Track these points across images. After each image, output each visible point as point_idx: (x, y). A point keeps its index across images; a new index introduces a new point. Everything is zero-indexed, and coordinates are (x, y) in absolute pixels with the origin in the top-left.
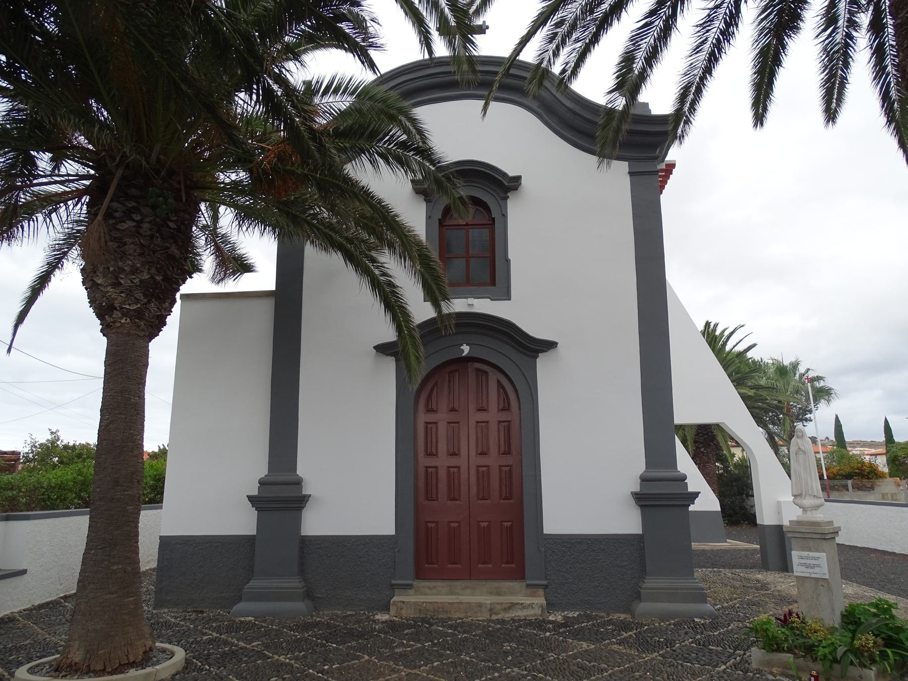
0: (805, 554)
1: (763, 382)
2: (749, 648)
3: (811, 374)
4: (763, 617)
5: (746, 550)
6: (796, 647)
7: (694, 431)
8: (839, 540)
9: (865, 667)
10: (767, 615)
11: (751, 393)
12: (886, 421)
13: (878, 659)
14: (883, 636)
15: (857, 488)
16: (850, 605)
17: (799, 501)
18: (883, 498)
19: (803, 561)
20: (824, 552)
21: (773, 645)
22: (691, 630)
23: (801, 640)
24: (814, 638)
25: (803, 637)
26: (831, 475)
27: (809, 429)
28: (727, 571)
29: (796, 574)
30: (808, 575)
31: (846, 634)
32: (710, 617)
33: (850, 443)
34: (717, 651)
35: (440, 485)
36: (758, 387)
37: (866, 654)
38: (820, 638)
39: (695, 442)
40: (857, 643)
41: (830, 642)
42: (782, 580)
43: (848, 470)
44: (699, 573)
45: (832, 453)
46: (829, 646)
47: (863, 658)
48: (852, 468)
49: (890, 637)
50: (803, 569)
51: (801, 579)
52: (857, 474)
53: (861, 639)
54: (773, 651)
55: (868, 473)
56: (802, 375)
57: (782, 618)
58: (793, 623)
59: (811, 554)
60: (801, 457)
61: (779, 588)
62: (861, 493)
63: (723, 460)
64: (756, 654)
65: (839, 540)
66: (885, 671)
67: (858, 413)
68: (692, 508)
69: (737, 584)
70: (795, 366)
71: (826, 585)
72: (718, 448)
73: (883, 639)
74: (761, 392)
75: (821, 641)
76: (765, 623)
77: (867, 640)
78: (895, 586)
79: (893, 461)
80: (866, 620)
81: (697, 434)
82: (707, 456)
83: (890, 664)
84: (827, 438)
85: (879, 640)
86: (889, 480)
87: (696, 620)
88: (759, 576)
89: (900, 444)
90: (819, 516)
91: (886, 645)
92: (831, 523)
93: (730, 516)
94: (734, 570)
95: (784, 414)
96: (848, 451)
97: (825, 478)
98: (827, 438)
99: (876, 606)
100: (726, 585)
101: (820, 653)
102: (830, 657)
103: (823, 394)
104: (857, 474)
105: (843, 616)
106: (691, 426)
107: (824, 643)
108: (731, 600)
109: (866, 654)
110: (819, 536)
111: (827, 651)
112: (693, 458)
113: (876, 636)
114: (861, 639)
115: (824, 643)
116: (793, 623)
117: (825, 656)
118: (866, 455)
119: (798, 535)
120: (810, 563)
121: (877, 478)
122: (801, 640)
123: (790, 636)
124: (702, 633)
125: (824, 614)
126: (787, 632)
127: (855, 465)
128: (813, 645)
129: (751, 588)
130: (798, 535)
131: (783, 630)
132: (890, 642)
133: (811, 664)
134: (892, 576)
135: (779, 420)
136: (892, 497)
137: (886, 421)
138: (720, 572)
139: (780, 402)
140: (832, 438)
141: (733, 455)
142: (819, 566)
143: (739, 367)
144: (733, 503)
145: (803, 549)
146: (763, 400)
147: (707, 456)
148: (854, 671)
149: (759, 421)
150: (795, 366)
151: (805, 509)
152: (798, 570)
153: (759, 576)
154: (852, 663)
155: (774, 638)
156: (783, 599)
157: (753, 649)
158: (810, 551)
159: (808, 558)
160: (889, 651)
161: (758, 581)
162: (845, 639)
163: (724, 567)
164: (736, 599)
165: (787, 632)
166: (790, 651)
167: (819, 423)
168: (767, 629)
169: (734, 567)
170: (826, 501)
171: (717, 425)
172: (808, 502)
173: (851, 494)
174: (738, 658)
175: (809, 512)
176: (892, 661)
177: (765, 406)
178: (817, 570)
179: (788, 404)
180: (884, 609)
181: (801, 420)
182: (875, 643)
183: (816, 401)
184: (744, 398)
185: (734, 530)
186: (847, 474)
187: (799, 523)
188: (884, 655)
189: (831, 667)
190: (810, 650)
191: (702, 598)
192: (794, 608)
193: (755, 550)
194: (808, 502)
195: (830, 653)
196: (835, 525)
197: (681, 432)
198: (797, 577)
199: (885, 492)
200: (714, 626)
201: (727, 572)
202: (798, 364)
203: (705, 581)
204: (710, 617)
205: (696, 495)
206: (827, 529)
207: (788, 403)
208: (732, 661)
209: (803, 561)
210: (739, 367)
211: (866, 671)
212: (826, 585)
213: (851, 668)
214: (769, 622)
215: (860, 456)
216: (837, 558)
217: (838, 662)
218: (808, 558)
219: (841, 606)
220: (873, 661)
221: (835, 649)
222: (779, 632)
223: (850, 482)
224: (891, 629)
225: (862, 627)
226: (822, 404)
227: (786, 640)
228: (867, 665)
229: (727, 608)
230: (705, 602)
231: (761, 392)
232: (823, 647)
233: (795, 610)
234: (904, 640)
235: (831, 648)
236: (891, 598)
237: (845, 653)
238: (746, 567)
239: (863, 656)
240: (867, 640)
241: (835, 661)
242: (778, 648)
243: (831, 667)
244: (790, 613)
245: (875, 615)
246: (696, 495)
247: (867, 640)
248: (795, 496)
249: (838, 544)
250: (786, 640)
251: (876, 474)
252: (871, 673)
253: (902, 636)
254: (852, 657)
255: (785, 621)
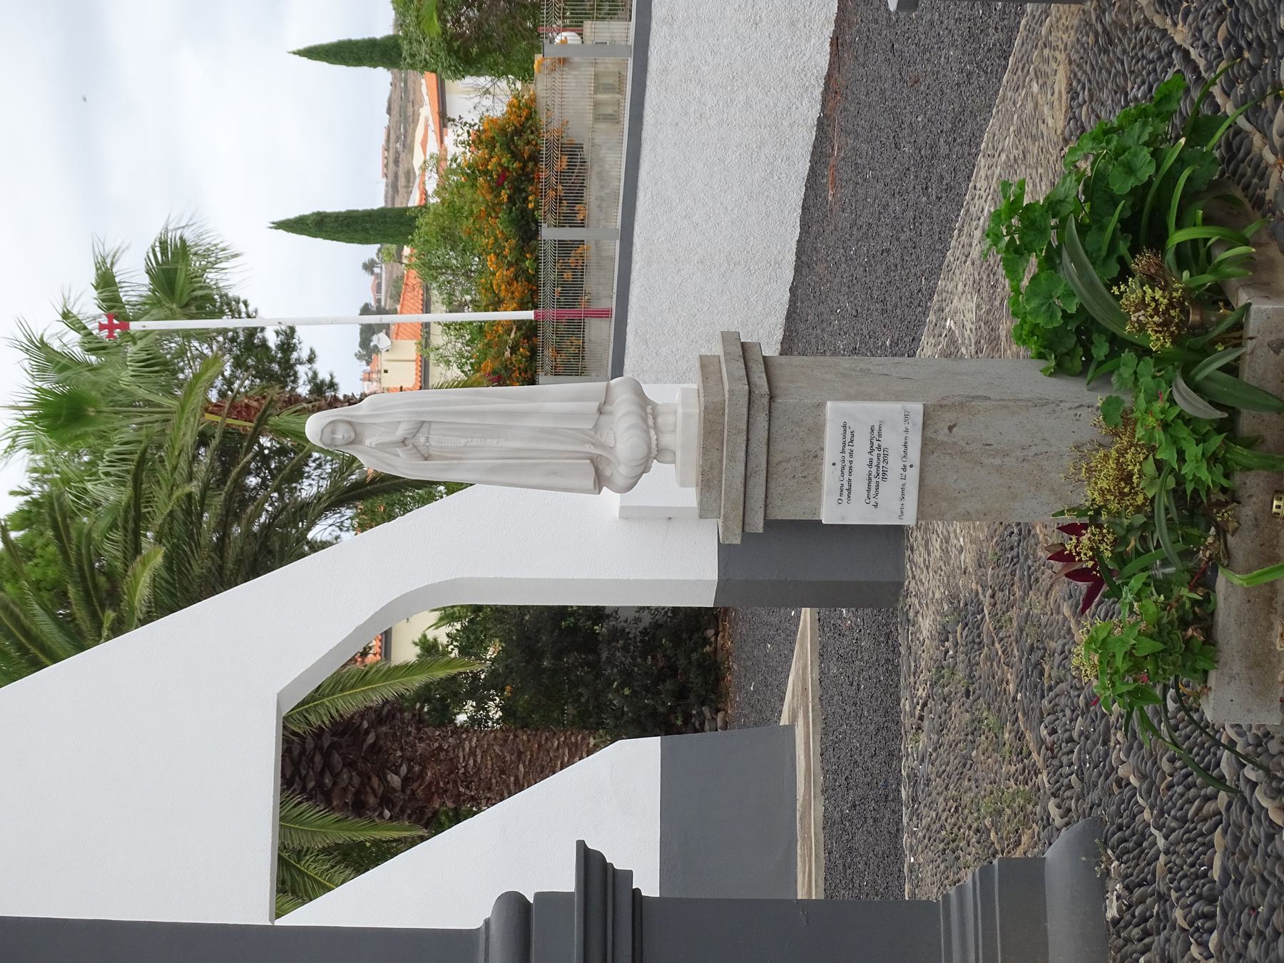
0: (830, 477)
1: (109, 493)
2: (1202, 726)
3: (89, 307)
4: (1083, 659)
5: (823, 654)
6: (1186, 555)
7: (311, 812)
8: (771, 349)
9: (1239, 326)
10: (1086, 643)
11: (154, 556)
12: (313, 53)
13: (1208, 279)
14: (1123, 248)
15: (571, 206)
16: (1021, 340)
17: (621, 472)
18: (614, 119)
19: (859, 487)
20: (820, 406)
21: (1187, 640)
22: (1157, 941)
23: (1161, 533)
24: (1149, 489)
25: (1148, 525)
26: (518, 287)
27: (331, 354)
28: (908, 746)
29: (909, 519)
30: (913, 474)
31: (1126, 372)
32: (1096, 856)
33: (393, 188)
34: (1228, 853)
35: (743, 454)
36: (133, 520)
37: (1194, 317)
38: (1150, 468)
39: (359, 808)
40: (1157, 341)
41: (1159, 435)
42: (936, 544)
43: (499, 225)
44: (923, 876)
45: (431, 271)
46: (1175, 441)
47: (1203, 331)
48: (492, 209)
49: (1127, 225)
50: (889, 490)
51: (930, 499)
52: (518, 194)
53: (1142, 327)
54: (1210, 639)
55: (515, 156)
56: (93, 346)
57: (1083, 586)
58: (1097, 552)
59: (831, 452)
60: (436, 440)
61: (968, 559)
62: (593, 192)
63: (442, 699)
64: (1226, 704)
65: (771, 349)
66: (1248, 262)
67: (263, 142)
68: (648, 883)
69: (960, 718)
70: (46, 357)
71: (949, 417)
72: (386, 715)
73: (1135, 250)
74: (163, 504)
75: (1159, 465)
76: (1108, 660)
77: (1141, 304)
78: (944, 149)
79: (465, 56)
80: (1070, 294)
81: (324, 796)
82: (424, 761)
83: (1226, 244)
84: (369, 267)
85: (1141, 263)
86: (541, 86)
87: (1112, 913)
88: (926, 625)
89: (400, 24)
90: (678, 398)
91: (1158, 240)
92: (706, 364)
93: (681, 694)
94: (907, 722)
95: (257, 433)
96: (424, 208)
97: (529, 315)
98: (369, 267)
99: (1016, 253)
100: (966, 762)
101: (1205, 475)
102: (1216, 441)
103: (180, 277)
104: (518, 194)
105: (1060, 370)
106: (286, 821)
107: (1167, 454)
108: (1023, 754)
109: (1194, 317)
110: (759, 481)
111: (1193, 450)
112: (440, 828)
113: (1125, 274)
114: (1142, 327)
115: (1167, 454)
116: (1097, 552)
117: (1212, 459)
118: (440, 150)
119: (758, 493)
120: (864, 456)
121: (535, 130)
122: (1161, 533)
123: (1153, 561)
124: (1162, 898)
125: (1058, 442)
126: (1136, 583)
127: (480, 197)
128: (1178, 493)
129: (972, 665)
130: (758, 493)
131: (1128, 596)
132: (1144, 224)
133: (1247, 512)
134: (907, 149)
135: (282, 451)
136: (608, 89)
137: (313, 53)
138: (913, 777)
139: (203, 439)
140: (370, 251)
141: (429, 648)
142: (876, 433)
143: (37, 586)
144: (627, 677)
145: (813, 481)
146: (191, 509)
147: (424, 761)
148: (1259, 365)
149: (275, 547)
150: (46, 357)
151: (652, 454)
152: (895, 506)
153: (926, 625)
154: (1232, 370)
155: (1159, 631)
156: (1011, 546)
157: (1209, 716)
158: (817, 456)
159: (846, 468)
160: (1177, 237)
161: (944, 634)
162: (1146, 380)
163: (894, 756)
164: (1020, 736)
165: (1136, 583)
166: (1203, 580)
167: (308, 298)
168: (1129, 654)
169: (891, 713)
170: (618, 370)
171: (286, 723)
172: (623, 438)
173: (598, 233)
174: (1250, 773)
175: (667, 440)
176: (1212, 234)
177: (218, 500)
178: (892, 440)
179: (216, 409)
180: (1025, 229)
181: (288, 367)
182: (1151, 280)
183: (206, 302)
184: (178, 592)
185: (742, 686)
186: (518, 251)
187: (708, 482)
188: (1192, 256)
189: (1250, 444)
190: (1194, 509)
191: (1019, 883)
192: (1046, 535)
193: (821, 623)
194: (623, 438)
195: (1202, 439)
196: (717, 350)
197: (311, 868)
198: (921, 514)
199: (587, 105)
200: (1134, 844)
201: (914, 746)
202: (43, 346)
203: (951, 848)
204: (1096, 856)
205: (589, 861)
206: (731, 383)
207: (209, 408)
208: (1261, 797)
209: (859, 487)
210: (37, 586)
211: (1253, 326)
212: (949, 417)
213: (1246, 374)
214: (1102, 645)
215: (444, 177)
216: (846, 362)
217: (1233, 412)
218: (846, 468)
219: (1023, 373)
220: (1218, 296)
221: (1188, 421)
222: (1132, 614)
223: (549, 233)
224: (1097, 218)
225: (1096, 312)
226: (231, 279)
227: (1163, 586)
228: (1231, 318)
229: (1055, 772)
230: (1036, 866)
231: (163, 504)
232: (1181, 458)
233: (1055, 538)
234: (1132, 183)
235: (1183, 432)
236: (982, 202)
237: (1197, 388)
238: (893, 669)
239: (1202, 328)
240: (1142, 305)
241: (1227, 427)
242: (1197, 619)
243: (1250, 444)
244: (1060, 555)
245: (1051, 261)
246: (589, 861)
247: (1141, 304)
248: (600, 481)
249: (788, 346)
250: (1163, 586)
251: (519, 132)
252: (1262, 311)
253: (1122, 185)
254: (1210, 368)
255: (1096, 582)
